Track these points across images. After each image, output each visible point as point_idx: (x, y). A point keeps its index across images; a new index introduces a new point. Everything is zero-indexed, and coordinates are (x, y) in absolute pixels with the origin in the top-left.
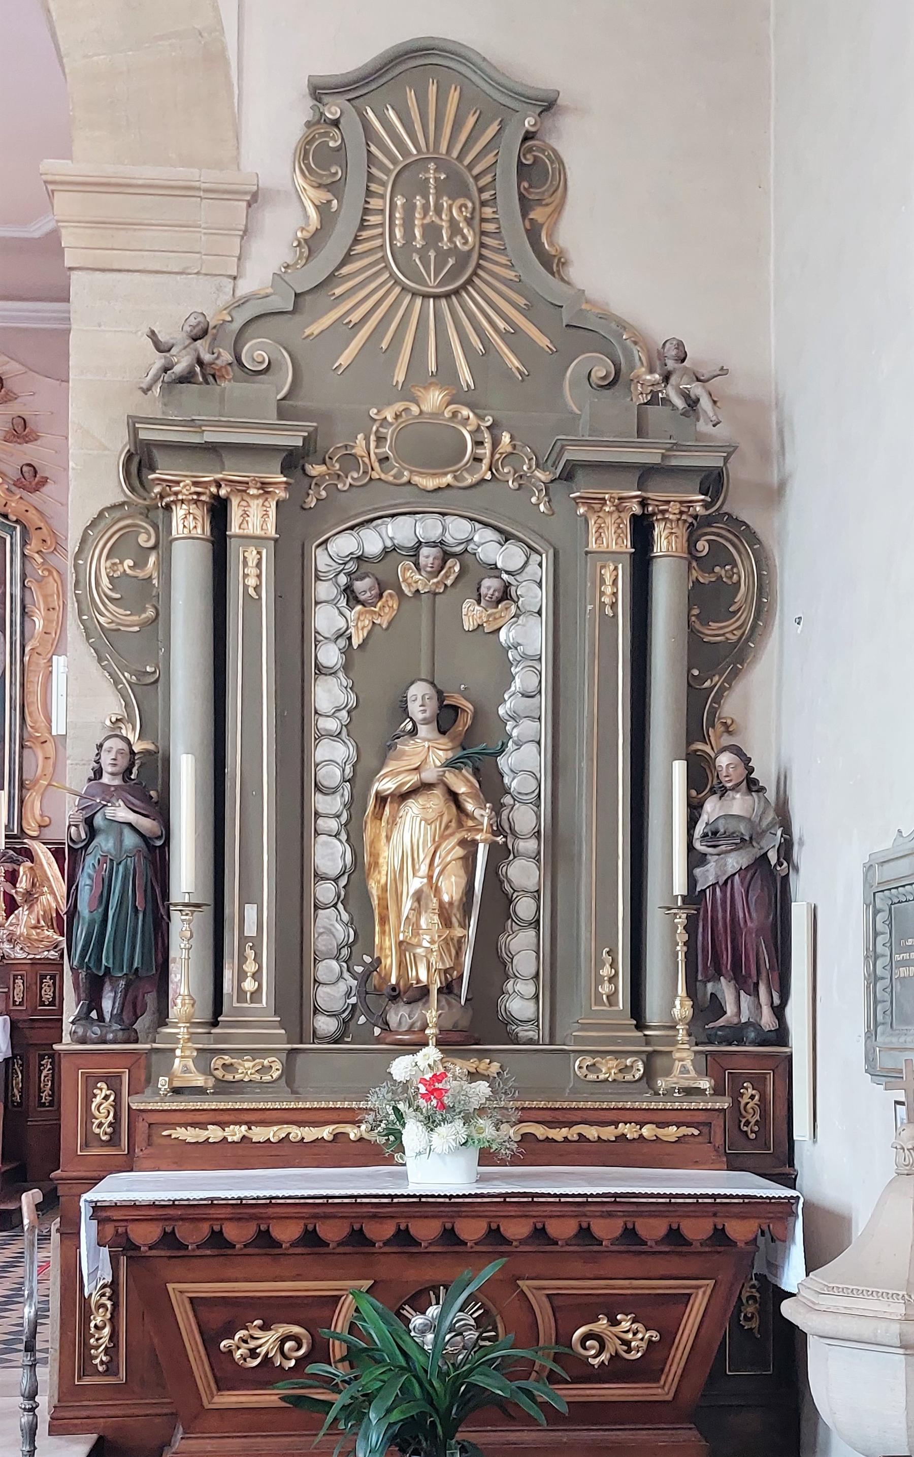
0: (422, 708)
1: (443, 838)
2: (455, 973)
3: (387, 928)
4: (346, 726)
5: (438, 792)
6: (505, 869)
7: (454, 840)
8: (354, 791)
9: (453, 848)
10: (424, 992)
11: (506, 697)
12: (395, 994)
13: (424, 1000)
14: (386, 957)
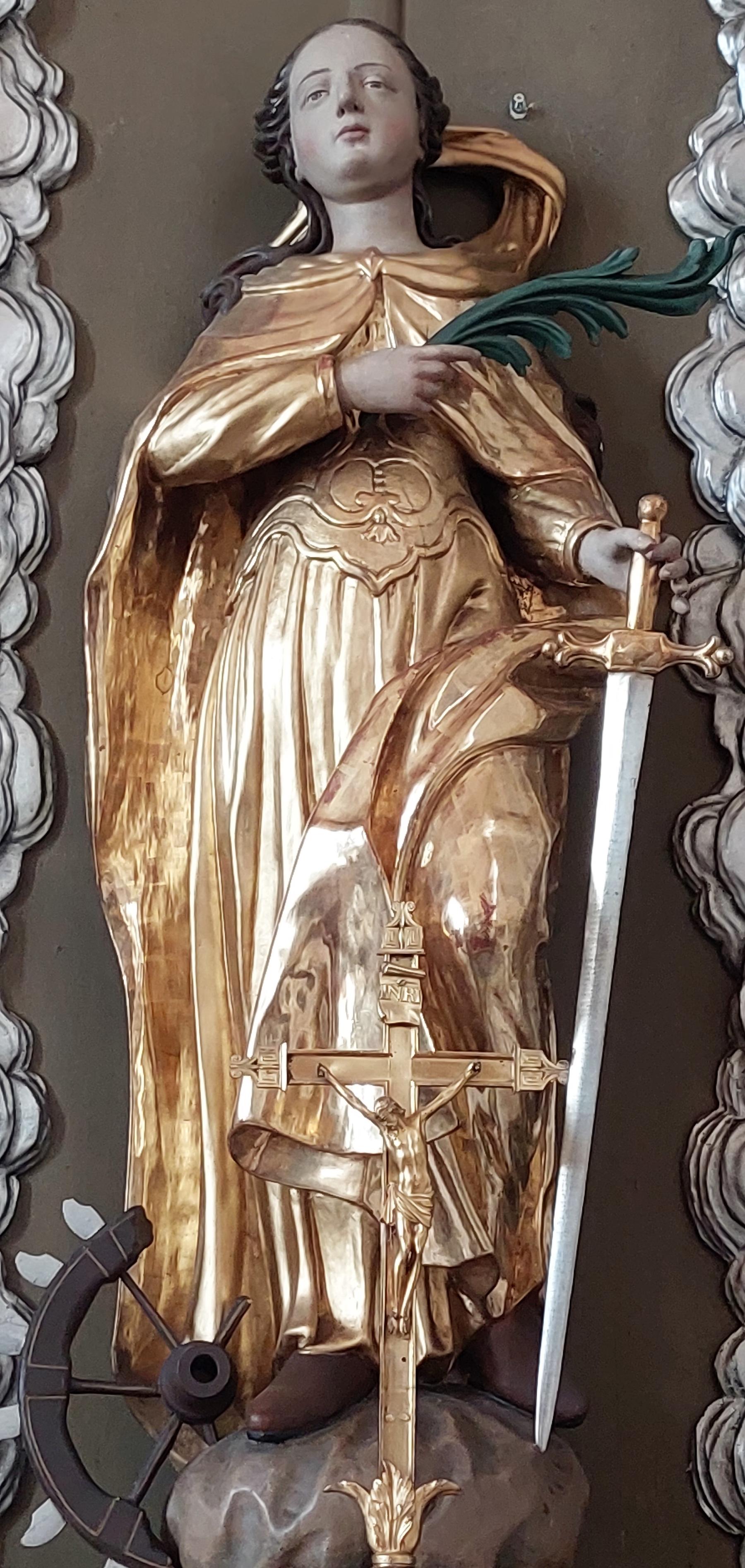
0: (349, 119)
1: (445, 653)
2: (502, 1287)
3: (185, 1080)
4: (31, 244)
5: (424, 458)
6: (706, 833)
7: (487, 663)
8: (62, 509)
9: (491, 692)
10: (353, 1380)
11: (698, 144)
12: (211, 1395)
13: (349, 1426)
14: (179, 1216)
